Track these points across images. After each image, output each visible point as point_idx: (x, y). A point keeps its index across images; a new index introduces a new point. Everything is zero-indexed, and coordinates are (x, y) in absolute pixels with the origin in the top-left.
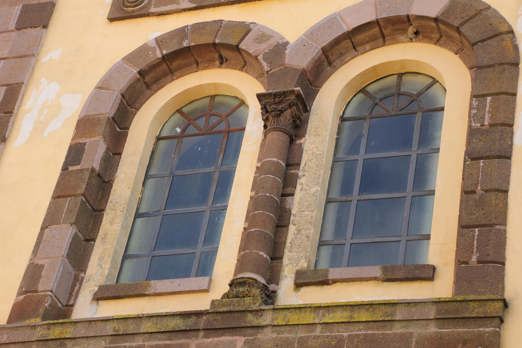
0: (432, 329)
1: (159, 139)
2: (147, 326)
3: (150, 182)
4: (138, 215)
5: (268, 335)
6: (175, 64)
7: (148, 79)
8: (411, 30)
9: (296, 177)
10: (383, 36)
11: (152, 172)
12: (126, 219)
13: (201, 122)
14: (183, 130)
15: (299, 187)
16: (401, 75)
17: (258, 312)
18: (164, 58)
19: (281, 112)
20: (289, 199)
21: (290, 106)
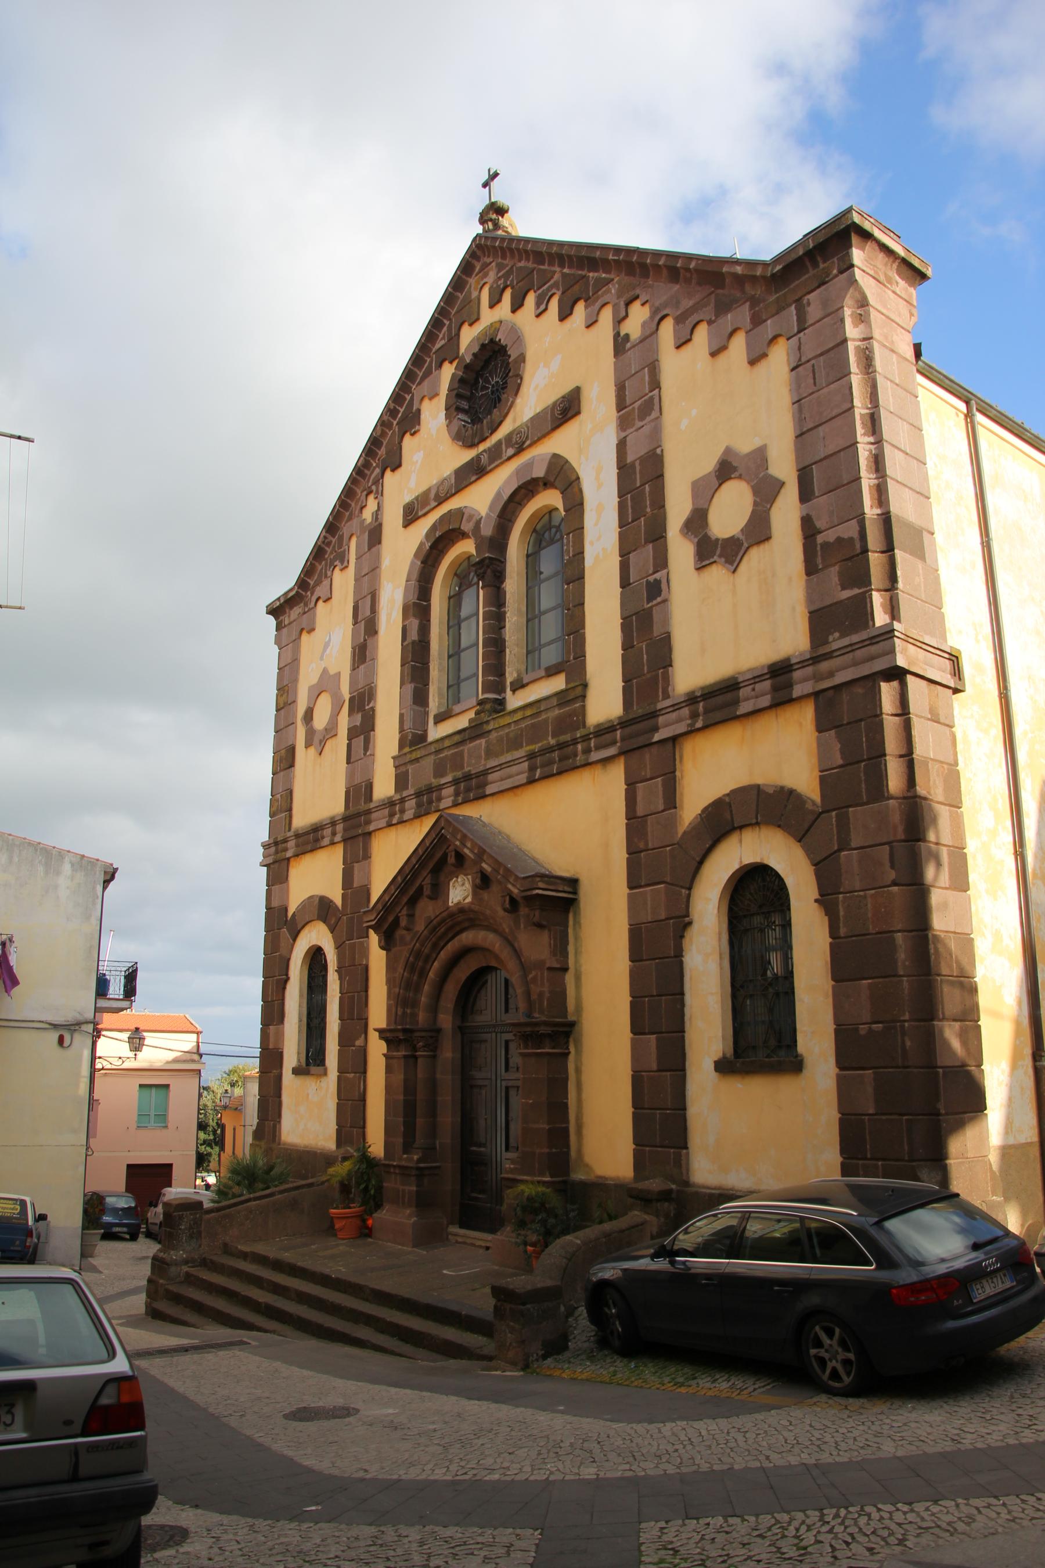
0: (557, 712)
1: (450, 598)
2: (447, 743)
3: (451, 630)
4: (449, 657)
5: (494, 735)
6: (440, 547)
7: (430, 563)
8: (541, 484)
9: (505, 613)
10: (532, 491)
11: (451, 624)
12: (440, 664)
13: (547, 535)
14: (459, 588)
15: (507, 620)
16: (550, 512)
17: (487, 722)
18: (431, 547)
19: (485, 573)
20: (503, 630)
21: (488, 567)
